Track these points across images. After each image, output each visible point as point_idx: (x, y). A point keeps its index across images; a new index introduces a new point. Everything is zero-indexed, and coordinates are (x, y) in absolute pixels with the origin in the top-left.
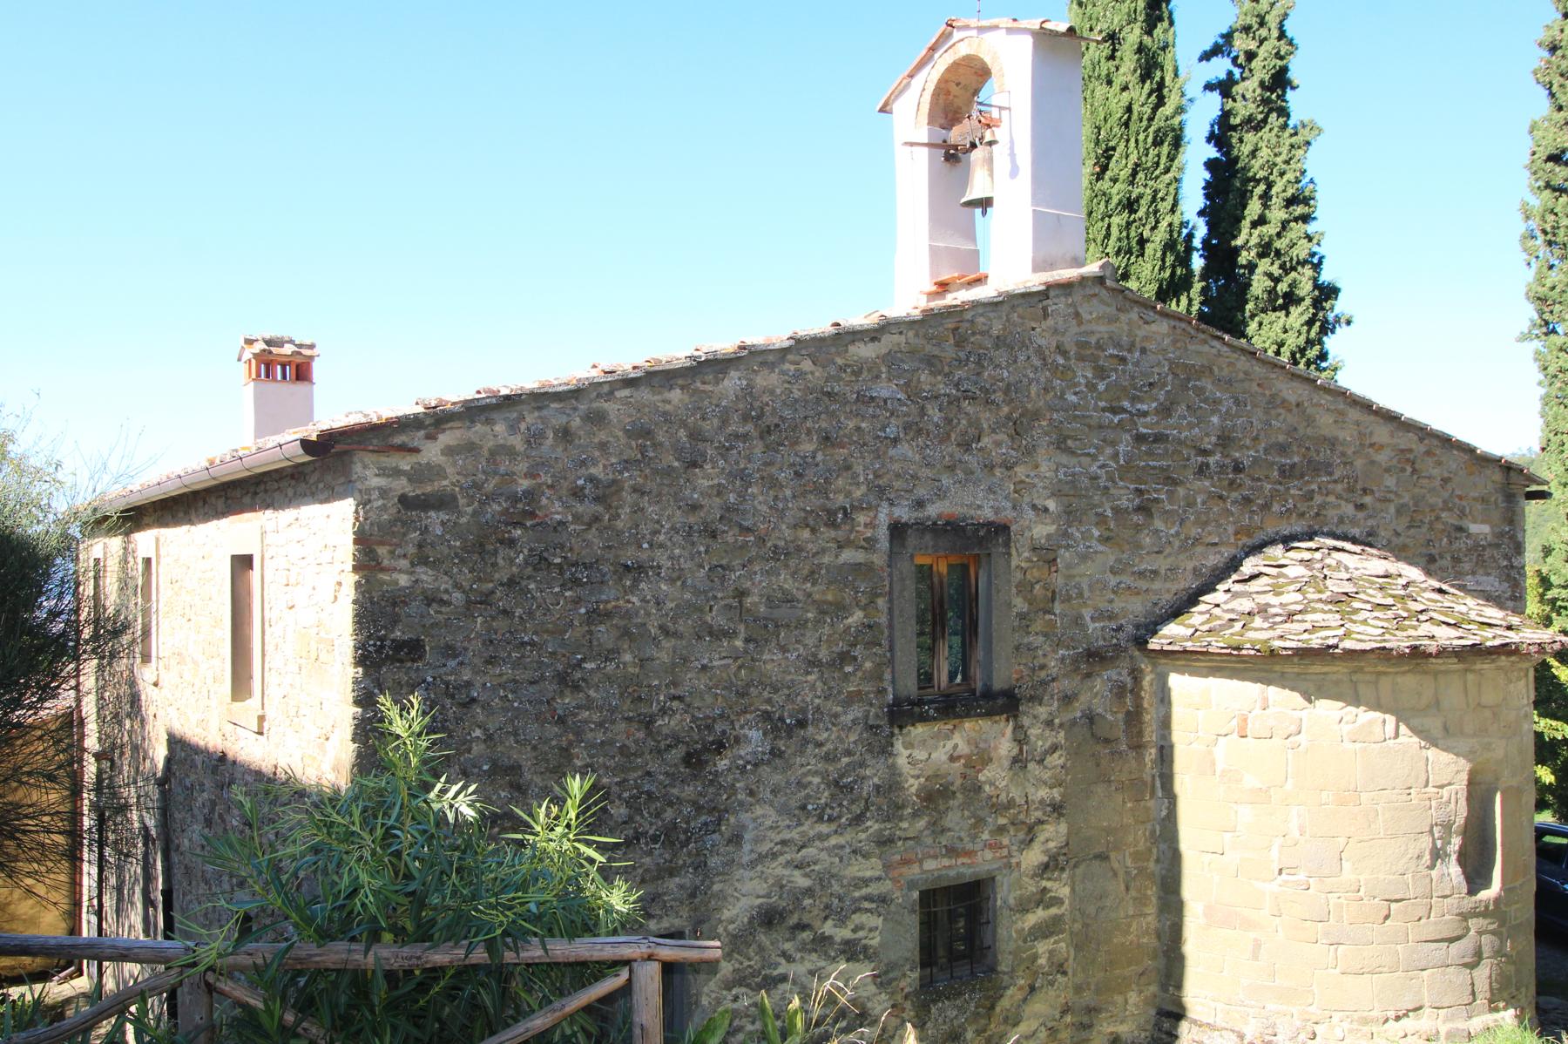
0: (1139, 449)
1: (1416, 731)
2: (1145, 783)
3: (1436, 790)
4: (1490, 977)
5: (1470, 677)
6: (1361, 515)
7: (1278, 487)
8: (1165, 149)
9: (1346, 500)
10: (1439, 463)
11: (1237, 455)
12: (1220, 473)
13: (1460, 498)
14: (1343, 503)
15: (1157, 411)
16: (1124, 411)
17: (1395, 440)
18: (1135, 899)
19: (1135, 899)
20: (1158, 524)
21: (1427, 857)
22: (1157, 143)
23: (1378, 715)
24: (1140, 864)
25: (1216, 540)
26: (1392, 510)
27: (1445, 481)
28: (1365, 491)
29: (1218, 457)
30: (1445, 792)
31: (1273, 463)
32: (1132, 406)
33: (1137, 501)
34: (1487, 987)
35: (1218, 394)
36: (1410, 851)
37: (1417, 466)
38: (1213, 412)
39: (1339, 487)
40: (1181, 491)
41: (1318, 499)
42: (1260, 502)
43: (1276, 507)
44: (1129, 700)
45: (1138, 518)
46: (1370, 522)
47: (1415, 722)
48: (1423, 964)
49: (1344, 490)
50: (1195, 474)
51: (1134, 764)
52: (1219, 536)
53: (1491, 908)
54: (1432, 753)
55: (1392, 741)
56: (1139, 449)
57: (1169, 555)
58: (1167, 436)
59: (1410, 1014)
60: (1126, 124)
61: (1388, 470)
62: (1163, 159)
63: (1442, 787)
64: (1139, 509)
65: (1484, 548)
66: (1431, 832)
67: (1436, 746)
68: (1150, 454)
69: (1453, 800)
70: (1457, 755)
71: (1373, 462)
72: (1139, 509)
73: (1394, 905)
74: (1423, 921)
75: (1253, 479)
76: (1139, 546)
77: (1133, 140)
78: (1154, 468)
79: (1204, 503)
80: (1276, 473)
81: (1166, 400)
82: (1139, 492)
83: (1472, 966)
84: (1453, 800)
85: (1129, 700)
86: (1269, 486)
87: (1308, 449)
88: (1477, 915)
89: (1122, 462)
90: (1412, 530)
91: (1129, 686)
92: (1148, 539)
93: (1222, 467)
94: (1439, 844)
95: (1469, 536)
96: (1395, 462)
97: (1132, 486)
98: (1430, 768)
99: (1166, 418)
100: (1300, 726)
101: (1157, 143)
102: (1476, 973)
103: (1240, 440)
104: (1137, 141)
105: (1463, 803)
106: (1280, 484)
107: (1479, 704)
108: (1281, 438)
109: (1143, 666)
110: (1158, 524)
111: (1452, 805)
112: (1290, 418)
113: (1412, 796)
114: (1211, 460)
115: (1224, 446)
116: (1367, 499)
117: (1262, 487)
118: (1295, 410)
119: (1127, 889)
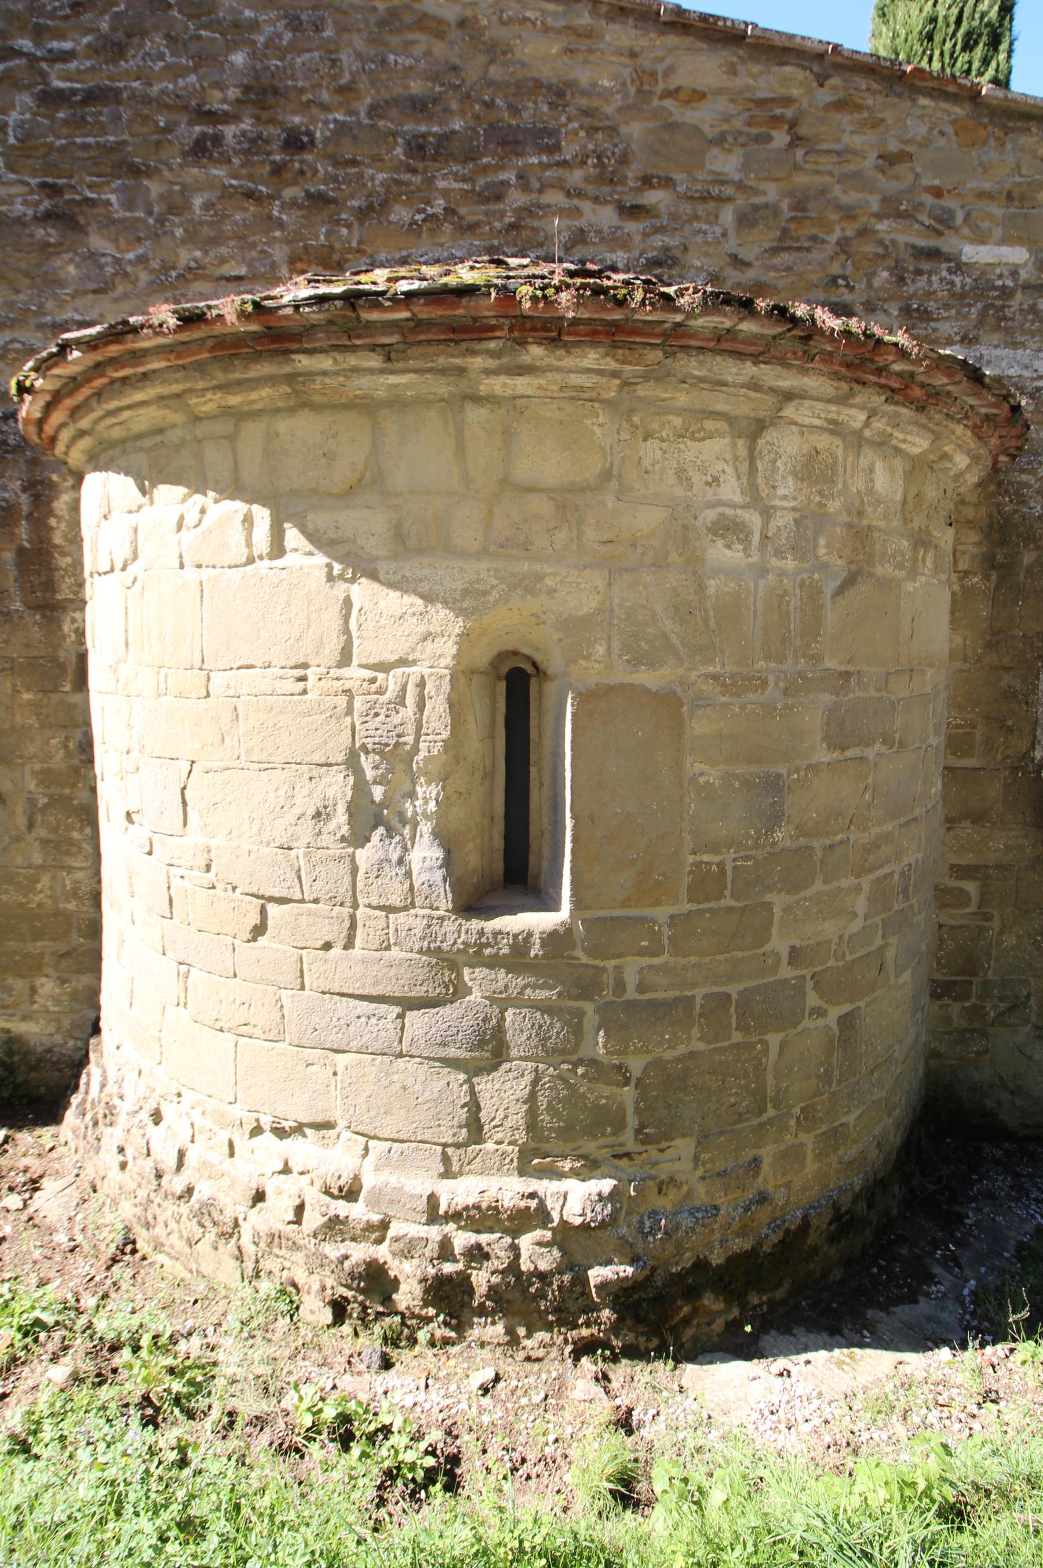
0: (52, 118)
1: (318, 540)
2: (62, 667)
3: (368, 674)
4: (532, 1098)
5: (475, 414)
6: (633, 227)
7: (407, 177)
8: (979, 52)
9: (596, 200)
10: (876, 124)
11: (297, 120)
12: (247, 152)
13: (937, 193)
14: (586, 206)
15: (93, 50)
16: (19, 53)
17: (742, 81)
18: (45, 842)
19: (45, 842)
20: (98, 242)
21: (341, 818)
22: (968, 46)
23: (236, 508)
24: (54, 790)
25: (243, 271)
26: (728, 215)
27: (890, 160)
28: (647, 181)
29: (246, 124)
30: (392, 681)
31: (394, 134)
32: (38, 44)
33: (46, 204)
34: (517, 1117)
35: (248, 13)
36: (298, 800)
37: (803, 130)
38: (233, 46)
39: (576, 177)
40: (155, 188)
41: (516, 199)
42: (355, 203)
43: (400, 213)
44: (23, 531)
45: (51, 234)
46: (658, 241)
47: (319, 520)
48: (334, 1039)
49: (587, 180)
50: (184, 155)
51: (36, 633)
52: (250, 266)
53: (535, 950)
54: (362, 591)
55: (267, 563)
56: (52, 118)
57: (126, 296)
58: (118, 92)
59: (308, 1131)
60: (930, 37)
61: (720, 141)
62: (976, 65)
63: (384, 667)
64: (49, 217)
65: (1006, 293)
66: (352, 761)
67: (373, 576)
68: (77, 123)
69: (410, 700)
70: (428, 598)
71: (673, 127)
72: (49, 217)
73: (272, 909)
74: (336, 951)
75: (336, 163)
76: (55, 282)
77: (937, 53)
78: (85, 147)
79: (207, 206)
80: (399, 151)
81: (114, 29)
82: (52, 190)
83: (473, 1069)
84: (410, 700)
85: (23, 531)
86: (381, 177)
87: (489, 105)
88: (494, 963)
89: (12, 141)
90: (786, 258)
91: (25, 509)
92: (72, 269)
93: (254, 144)
94: (378, 793)
95: (959, 267)
96: (738, 124)
97: (34, 181)
98: (353, 625)
99: (115, 61)
100: (135, 544)
101: (968, 46)
102: (485, 1085)
103: (301, 91)
104: (942, 54)
105: (437, 709)
106: (414, 171)
107: (506, 482)
108: (416, 87)
109: (55, 477)
110: (98, 242)
111: (409, 711)
112: (439, 49)
113: (309, 684)
114: (229, 131)
115: (261, 105)
116: (654, 197)
117: (361, 176)
118: (455, 34)
119: (31, 825)
